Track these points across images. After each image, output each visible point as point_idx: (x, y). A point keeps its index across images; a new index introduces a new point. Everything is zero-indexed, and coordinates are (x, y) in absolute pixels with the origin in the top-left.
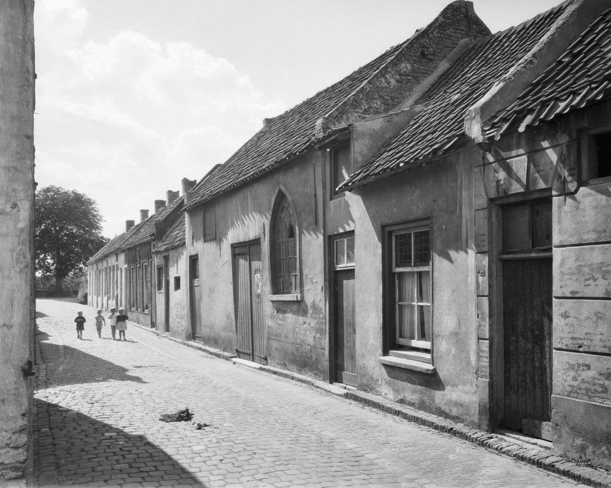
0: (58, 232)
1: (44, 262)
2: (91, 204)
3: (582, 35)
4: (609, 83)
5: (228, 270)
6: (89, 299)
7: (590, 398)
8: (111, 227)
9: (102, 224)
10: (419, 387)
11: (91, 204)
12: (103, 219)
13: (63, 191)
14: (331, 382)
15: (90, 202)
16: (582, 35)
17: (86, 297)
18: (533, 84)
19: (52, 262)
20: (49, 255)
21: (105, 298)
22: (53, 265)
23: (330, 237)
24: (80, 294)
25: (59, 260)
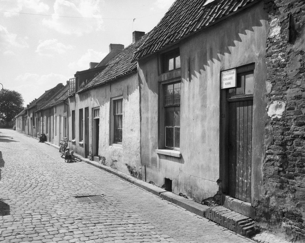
0: (8, 105)
1: (2, 116)
2: (19, 95)
3: (221, 2)
4: (304, 3)
5: (30, 120)
6: (16, 128)
7: (288, 181)
8: (26, 102)
9: (24, 102)
10: (253, 175)
11: (19, 95)
12: (24, 100)
13: (9, 91)
14: (85, 158)
15: (19, 95)
16: (180, 19)
17: (15, 128)
18: (190, 31)
19: (5, 116)
20: (4, 113)
21: (19, 128)
22: (5, 117)
23: (115, 101)
24: (14, 127)
25: (7, 115)
